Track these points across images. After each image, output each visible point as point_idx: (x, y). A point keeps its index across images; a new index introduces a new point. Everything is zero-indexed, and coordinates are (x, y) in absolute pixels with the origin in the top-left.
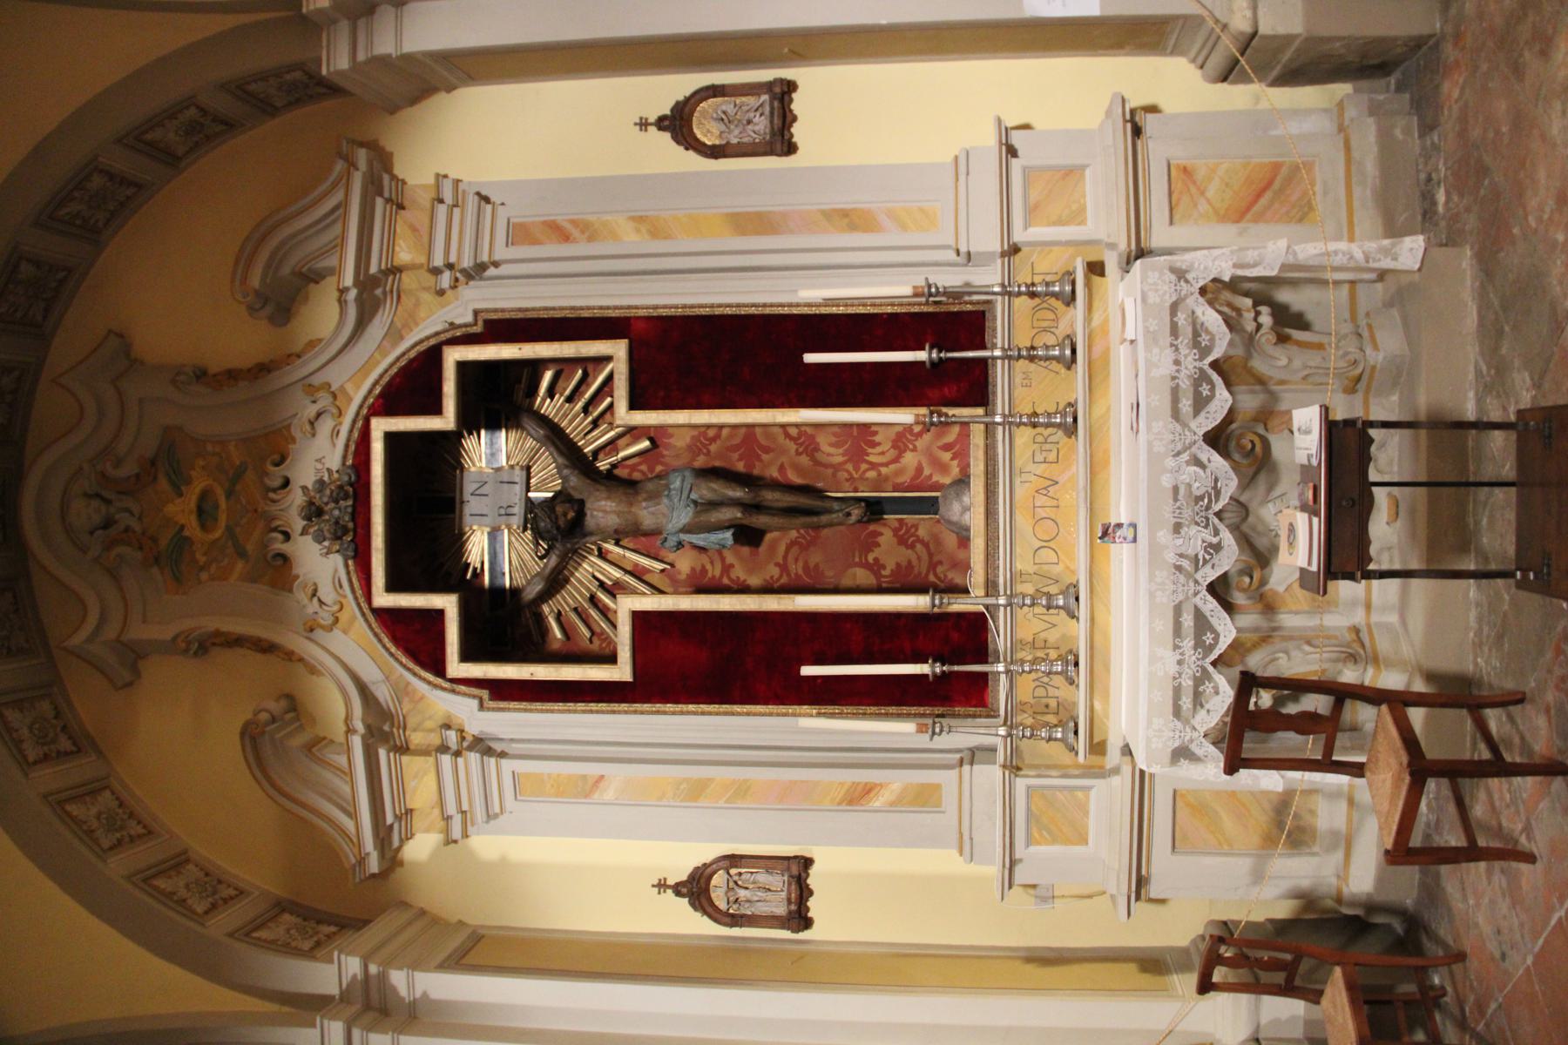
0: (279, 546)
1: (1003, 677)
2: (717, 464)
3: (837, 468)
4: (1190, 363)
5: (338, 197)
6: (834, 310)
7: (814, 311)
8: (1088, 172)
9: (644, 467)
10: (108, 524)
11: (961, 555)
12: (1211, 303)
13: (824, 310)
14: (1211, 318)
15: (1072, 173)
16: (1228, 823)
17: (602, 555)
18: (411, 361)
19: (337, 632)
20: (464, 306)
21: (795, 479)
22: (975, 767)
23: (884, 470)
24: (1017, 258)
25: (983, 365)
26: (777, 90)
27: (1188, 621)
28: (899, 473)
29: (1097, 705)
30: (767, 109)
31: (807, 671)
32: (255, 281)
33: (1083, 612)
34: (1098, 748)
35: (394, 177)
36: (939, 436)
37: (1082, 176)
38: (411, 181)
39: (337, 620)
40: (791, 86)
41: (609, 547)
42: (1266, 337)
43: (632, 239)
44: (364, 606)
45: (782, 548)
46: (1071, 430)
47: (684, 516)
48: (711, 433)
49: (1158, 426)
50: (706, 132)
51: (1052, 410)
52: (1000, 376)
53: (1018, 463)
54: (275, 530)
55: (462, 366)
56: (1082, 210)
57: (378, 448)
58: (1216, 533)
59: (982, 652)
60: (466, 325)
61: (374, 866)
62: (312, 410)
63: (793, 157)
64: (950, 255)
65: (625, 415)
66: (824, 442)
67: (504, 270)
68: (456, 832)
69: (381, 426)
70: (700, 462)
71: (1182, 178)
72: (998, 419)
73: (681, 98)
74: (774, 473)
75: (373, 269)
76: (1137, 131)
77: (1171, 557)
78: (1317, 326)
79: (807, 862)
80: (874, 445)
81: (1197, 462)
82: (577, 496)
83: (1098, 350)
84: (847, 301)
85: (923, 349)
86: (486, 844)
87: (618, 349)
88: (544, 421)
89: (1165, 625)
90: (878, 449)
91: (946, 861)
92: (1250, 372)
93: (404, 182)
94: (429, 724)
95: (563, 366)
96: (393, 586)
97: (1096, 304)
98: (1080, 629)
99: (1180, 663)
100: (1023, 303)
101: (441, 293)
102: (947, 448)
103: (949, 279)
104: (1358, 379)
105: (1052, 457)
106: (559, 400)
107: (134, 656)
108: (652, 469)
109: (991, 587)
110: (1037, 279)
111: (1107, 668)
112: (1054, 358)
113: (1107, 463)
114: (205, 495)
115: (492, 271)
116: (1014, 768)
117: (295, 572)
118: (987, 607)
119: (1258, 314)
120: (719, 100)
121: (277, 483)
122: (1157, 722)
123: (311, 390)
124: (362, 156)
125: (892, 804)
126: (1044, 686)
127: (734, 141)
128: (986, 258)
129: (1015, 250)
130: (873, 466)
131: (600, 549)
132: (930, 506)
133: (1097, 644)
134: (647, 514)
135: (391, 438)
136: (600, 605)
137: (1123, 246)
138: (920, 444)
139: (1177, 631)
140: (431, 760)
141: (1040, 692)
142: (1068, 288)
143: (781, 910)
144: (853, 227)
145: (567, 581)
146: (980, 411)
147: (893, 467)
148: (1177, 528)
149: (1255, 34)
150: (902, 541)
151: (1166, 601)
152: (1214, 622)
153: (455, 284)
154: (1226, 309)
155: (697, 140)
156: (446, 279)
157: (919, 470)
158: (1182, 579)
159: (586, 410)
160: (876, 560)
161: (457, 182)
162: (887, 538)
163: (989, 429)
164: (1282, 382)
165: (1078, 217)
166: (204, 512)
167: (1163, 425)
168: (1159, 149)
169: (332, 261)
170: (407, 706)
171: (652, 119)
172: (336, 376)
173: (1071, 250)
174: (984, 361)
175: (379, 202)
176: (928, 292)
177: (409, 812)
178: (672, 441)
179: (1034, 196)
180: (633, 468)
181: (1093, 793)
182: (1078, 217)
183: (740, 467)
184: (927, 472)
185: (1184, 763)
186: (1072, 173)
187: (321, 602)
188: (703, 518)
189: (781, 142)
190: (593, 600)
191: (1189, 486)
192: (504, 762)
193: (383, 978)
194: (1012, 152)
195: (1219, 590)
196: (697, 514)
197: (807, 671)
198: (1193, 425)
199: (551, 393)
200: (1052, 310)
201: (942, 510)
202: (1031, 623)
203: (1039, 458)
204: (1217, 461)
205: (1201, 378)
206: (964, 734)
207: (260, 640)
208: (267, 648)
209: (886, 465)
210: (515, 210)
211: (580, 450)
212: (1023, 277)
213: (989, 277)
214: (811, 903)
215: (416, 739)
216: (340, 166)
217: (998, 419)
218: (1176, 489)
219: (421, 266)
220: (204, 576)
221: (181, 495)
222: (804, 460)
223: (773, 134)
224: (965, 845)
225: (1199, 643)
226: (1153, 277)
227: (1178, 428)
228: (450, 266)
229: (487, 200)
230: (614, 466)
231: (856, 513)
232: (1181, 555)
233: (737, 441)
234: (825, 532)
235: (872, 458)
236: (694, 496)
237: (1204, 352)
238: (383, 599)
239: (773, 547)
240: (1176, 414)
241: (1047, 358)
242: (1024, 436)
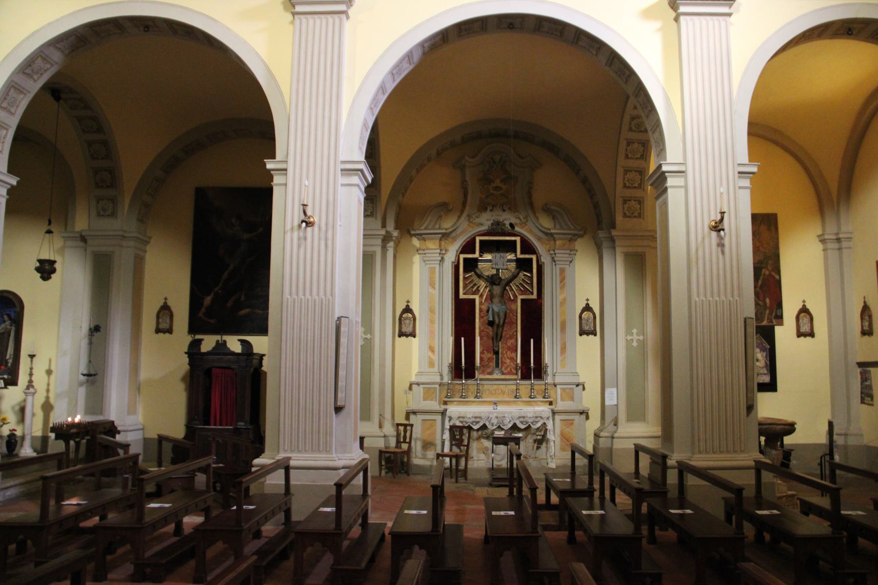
0: (489, 209)
1: (461, 382)
2: (507, 315)
3: (506, 344)
4: (530, 421)
5: (572, 227)
6: (543, 345)
7: (542, 341)
8: (572, 402)
9: (506, 298)
10: (494, 162)
11: (486, 373)
12: (542, 425)
13: (542, 343)
14: (539, 425)
15: (572, 399)
16: (429, 432)
17: (486, 287)
18: (533, 247)
19: (468, 223)
20: (546, 259)
21: (503, 334)
22: (439, 376)
23: (505, 355)
24: (553, 386)
25: (530, 378)
26: (594, 332)
27: (478, 420)
28: (505, 358)
29: (455, 403)
30: (590, 329)
31: (463, 339)
32: (552, 207)
33: (476, 400)
34: (445, 403)
35: (577, 239)
36: (514, 368)
37: (570, 400)
38: (576, 242)
39: (470, 222)
40: (595, 335)
41: (488, 289)
42: (535, 437)
43: (560, 298)
44: (476, 235)
45: (488, 330)
46: (516, 397)
47: (496, 309)
48: (515, 314)
49: (518, 414)
50: (586, 315)
51: (520, 393)
52: (528, 382)
53: (508, 386)
54: (493, 208)
55: (531, 260)
56: (564, 401)
57: (513, 238)
58: (496, 425)
59: (467, 378)
60: (541, 260)
61: (413, 232)
62: (522, 218)
63: (578, 335)
64: (555, 372)
65: (520, 297)
66: (512, 341)
67: (554, 266)
68: (420, 252)
69: (518, 239)
70: (508, 311)
71: (570, 423)
72: (518, 382)
73: (593, 309)
74: (505, 329)
75: (555, 236)
76: (581, 413)
77: (491, 416)
78: (537, 451)
79: (414, 337)
80: (511, 353)
81: (510, 422)
82: (501, 283)
83: (533, 403)
84: (544, 348)
85: (534, 365)
86: (417, 259)
87: (534, 296)
88: (518, 274)
89: (477, 415)
90: (510, 354)
91: (415, 369)
92: (528, 434)
93: (576, 241)
94: (446, 245)
95: (531, 278)
96: (481, 241)
97: (543, 403)
98: (472, 399)
99: (469, 418)
100: (543, 387)
101: (549, 251)
102: (511, 370)
103: (549, 370)
104: (526, 458)
105: (510, 393)
106: (523, 277)
107: (463, 169)
108: (506, 299)
109: (481, 380)
110: (549, 391)
111: (464, 405)
112: (531, 394)
113: (509, 405)
114: (500, 188)
115: (554, 263)
116: (441, 385)
117: (483, 213)
118: (477, 379)
119: (540, 436)
120: (593, 318)
121: (504, 208)
122: (457, 413)
123: (526, 218)
124: (581, 232)
125: (429, 357)
126: (459, 391)
127: (583, 322)
128: (554, 379)
129: (555, 386)
130: (507, 352)
131: (487, 286)
132: (497, 366)
133: (470, 403)
134: (496, 300)
135: (515, 242)
136: (540, 403)
137: (555, 409)
138: (512, 363)
139: (476, 417)
140: (438, 247)
141: (457, 391)
142: (546, 397)
143: (403, 330)
144: (562, 349)
145: (480, 279)
146: (520, 377)
147: (506, 357)
148: (497, 417)
149: (600, 437)
150: (489, 359)
151: (482, 415)
152: (478, 425)
153: (551, 254)
154: (541, 428)
155: (584, 312)
156: (552, 252)
157: (506, 363)
158: (486, 418)
159: (520, 284)
160: (484, 353)
161: (575, 255)
162: (490, 355)
163: (516, 380)
164: (526, 442)
165: (562, 400)
166: (497, 188)
167: (518, 415)
168: (577, 418)
169: (558, 226)
170: (450, 240)
171: (589, 302)
172: (530, 224)
173: (555, 398)
174: (531, 378)
175: (571, 236)
176: (547, 366)
177: (425, 240)
178: (513, 305)
179: (567, 390)
180: (507, 295)
181: (435, 402)
182: (562, 400)
183: (506, 321)
184: (505, 365)
185: (449, 419)
186: (572, 399)
187: (475, 219)
188: (496, 314)
189: (582, 333)
190: (475, 285)
191: (505, 420)
192: (438, 265)
193: (392, 240)
194: (577, 385)
195: (484, 427)
196: (497, 313)
197: (463, 339)
198: (517, 421)
199: (525, 275)
200: (542, 394)
201: (497, 369)
202: (473, 388)
203: (509, 391)
204: (510, 425)
205: (527, 423)
206: (446, 371)
207: (466, 203)
208: (464, 204)
209: (507, 355)
210: (568, 270)
211: (511, 282)
212: (549, 387)
213: (549, 380)
214: (404, 337)
215: (443, 243)
216: (579, 228)
217: (518, 382)
218: (504, 417)
219: (555, 247)
220: (481, 187)
221: (501, 182)
222: (508, 336)
223: (584, 331)
224: (420, 373)
225: (473, 422)
226: (547, 413)
227: (517, 417)
228: (555, 254)
229: (571, 262)
230: (507, 290)
231: (496, 349)
232: (491, 418)
233: (513, 320)
234: (491, 341)
235: (508, 352)
236: (501, 312)
237: (532, 423)
238: (478, 239)
239: (487, 328)
240: (519, 417)
241: (531, 392)
242: (514, 387)
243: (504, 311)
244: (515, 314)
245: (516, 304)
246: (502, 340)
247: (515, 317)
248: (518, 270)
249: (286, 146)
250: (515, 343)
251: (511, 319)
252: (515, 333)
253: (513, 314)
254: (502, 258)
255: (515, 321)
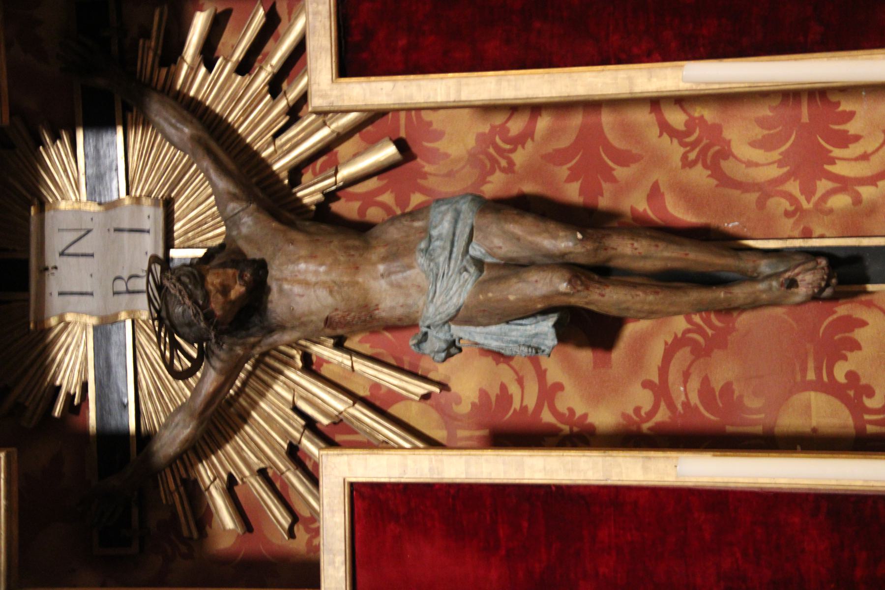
2: (529, 188)
3: (766, 190)
45: (657, 351)
80: (845, 140)
82: (252, 253)
90: (514, 389)
106: (224, 68)
130: (844, 184)
131: (307, 358)
145: (244, 418)
159: (275, 88)
160: (852, 376)
178: (441, 145)
180: (368, 199)
183: (572, 193)
188: (493, 294)
196: (481, 286)
211: (264, 166)
222: (699, 176)
230: (331, 196)
233: (565, 142)
234: (744, 320)
235: (840, 169)
243: (468, 214)
244: (516, 125)
245: (436, 120)
246: (731, 225)
247: (543, 123)
248: (158, 111)
249: (879, 235)
250: (764, 111)
251: (559, 157)
252: (676, 118)
253: (520, 140)
254: (82, 247)
255: (576, 120)
